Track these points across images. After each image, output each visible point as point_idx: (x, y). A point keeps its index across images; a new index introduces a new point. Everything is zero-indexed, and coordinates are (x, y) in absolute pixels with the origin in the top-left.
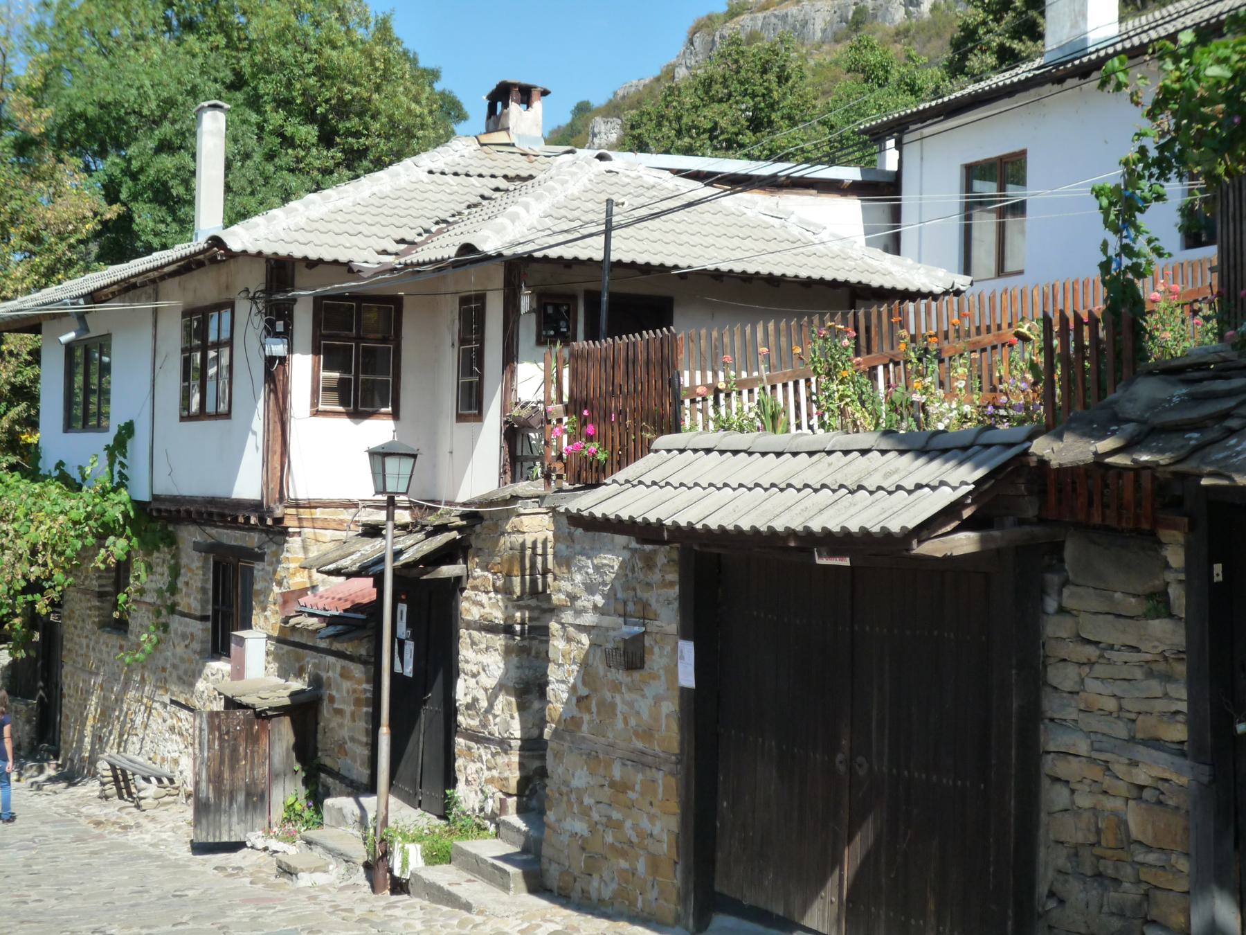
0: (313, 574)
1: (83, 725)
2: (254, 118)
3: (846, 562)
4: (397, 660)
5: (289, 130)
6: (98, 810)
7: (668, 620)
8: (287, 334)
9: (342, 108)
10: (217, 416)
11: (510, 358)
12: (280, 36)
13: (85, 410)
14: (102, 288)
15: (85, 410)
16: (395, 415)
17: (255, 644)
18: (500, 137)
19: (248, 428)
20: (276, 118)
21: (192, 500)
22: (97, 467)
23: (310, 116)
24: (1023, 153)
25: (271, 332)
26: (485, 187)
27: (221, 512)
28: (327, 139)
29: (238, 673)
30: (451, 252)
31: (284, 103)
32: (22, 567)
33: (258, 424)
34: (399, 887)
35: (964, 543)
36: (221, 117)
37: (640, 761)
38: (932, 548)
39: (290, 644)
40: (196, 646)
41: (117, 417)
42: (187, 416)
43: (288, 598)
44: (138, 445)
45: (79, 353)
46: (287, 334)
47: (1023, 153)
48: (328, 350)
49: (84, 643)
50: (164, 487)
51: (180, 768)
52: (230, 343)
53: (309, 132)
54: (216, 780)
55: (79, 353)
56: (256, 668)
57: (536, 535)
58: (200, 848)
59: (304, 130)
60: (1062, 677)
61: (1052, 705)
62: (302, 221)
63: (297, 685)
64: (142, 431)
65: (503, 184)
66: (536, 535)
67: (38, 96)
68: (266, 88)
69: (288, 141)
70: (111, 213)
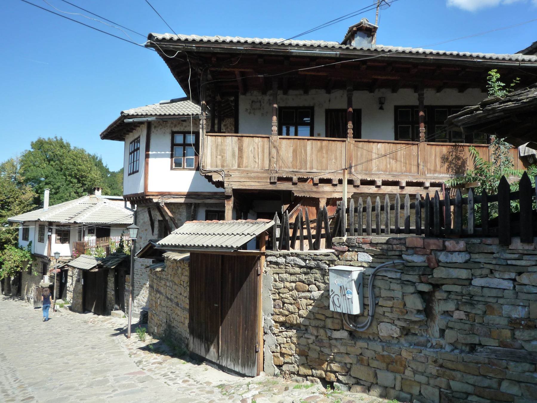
0: (54, 267)
2: (64, 177)
3: (452, 227)
4: (352, 263)
5: (72, 180)
6: (26, 304)
7: (81, 277)
8: (51, 232)
9: (82, 177)
11: (84, 236)
12: (70, 164)
13: (25, 238)
14: (34, 209)
15: (25, 238)
16: (69, 243)
17: (47, 277)
19: (46, 245)
20: (69, 178)
22: (26, 248)
23: (75, 177)
25: (49, 231)
26: (87, 206)
27: (42, 257)
28: (79, 182)
29: (44, 282)
30: (73, 222)
31: (70, 175)
32: (13, 264)
33: (47, 245)
34: (56, 311)
35: (97, 270)
38: (93, 271)
39: (51, 278)
41: (30, 240)
43: (51, 271)
44: (33, 244)
46: (51, 232)
48: (58, 233)
49: (25, 277)
50: (36, 252)
53: (75, 181)
54: (37, 298)
56: (46, 281)
58: (36, 308)
59: (74, 180)
62: (54, 215)
63: (51, 284)
64: (33, 242)
65: (91, 205)
67: (23, 175)
68: (67, 173)
69: (71, 182)
70: (37, 195)
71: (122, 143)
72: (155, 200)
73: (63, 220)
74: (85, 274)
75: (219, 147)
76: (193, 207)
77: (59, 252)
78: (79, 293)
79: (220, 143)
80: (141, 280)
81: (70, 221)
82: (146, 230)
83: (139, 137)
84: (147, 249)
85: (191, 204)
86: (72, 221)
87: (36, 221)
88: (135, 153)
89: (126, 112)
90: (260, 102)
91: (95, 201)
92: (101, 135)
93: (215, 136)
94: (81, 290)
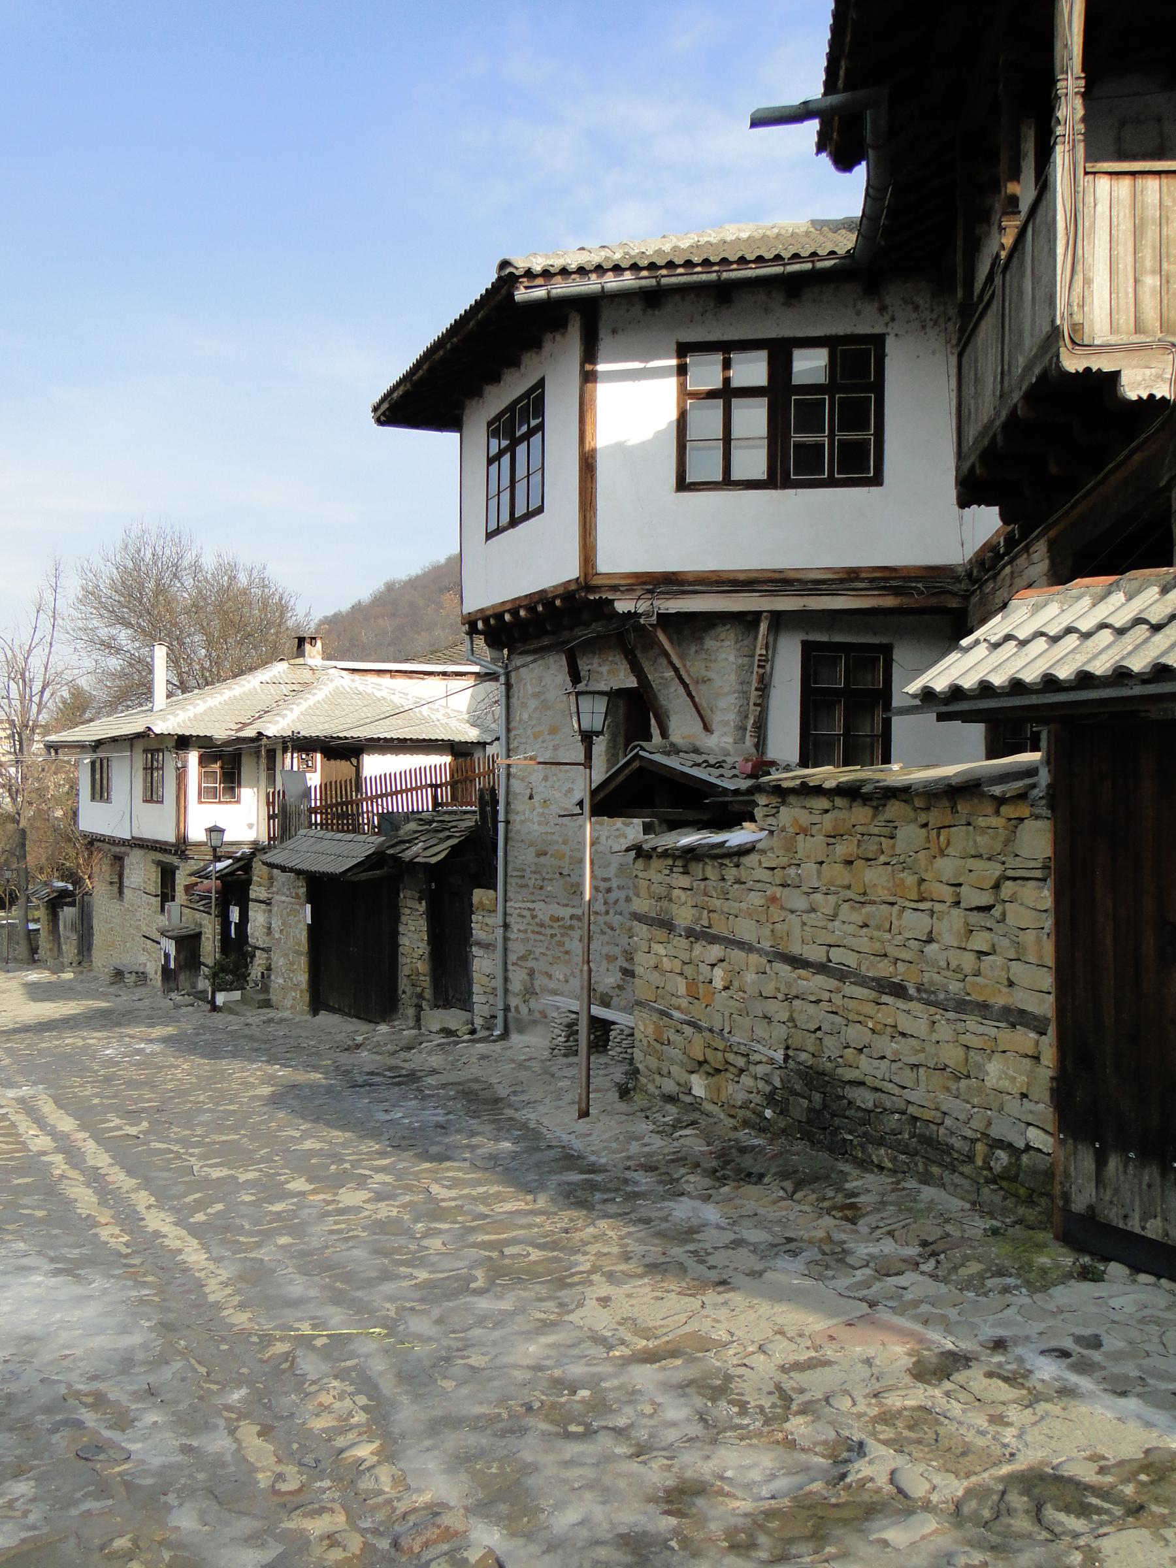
1: (701, 825)
10: (158, 802)
18: (300, 661)
21: (148, 840)
24: (1119, 371)
26: (285, 689)
36: (164, 649)
37: (297, 952)
40: (153, 909)
42: (145, 801)
45: (98, 765)
47: (1119, 371)
51: (567, 917)
52: (162, 769)
55: (98, 765)
57: (751, 704)
60: (404, 919)
61: (402, 929)
65: (295, 687)
66: (751, 704)
71: (449, 440)
72: (622, 606)
73: (220, 732)
74: (319, 888)
75: (1152, 232)
76: (763, 627)
77: (221, 825)
78: (297, 952)
79: (1153, 213)
80: (539, 906)
81: (242, 734)
82: (553, 730)
83: (541, 384)
84: (621, 778)
85: (757, 615)
86: (250, 733)
87: (138, 736)
88: (521, 450)
89: (521, 264)
90: (1159, 120)
91: (306, 675)
92: (375, 409)
93: (1133, 174)
94: (304, 947)
